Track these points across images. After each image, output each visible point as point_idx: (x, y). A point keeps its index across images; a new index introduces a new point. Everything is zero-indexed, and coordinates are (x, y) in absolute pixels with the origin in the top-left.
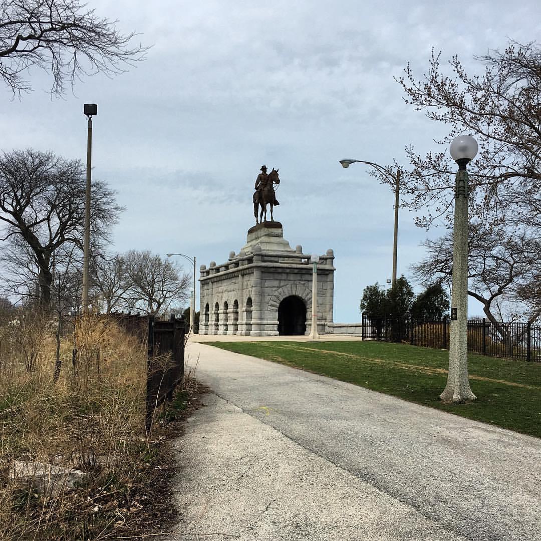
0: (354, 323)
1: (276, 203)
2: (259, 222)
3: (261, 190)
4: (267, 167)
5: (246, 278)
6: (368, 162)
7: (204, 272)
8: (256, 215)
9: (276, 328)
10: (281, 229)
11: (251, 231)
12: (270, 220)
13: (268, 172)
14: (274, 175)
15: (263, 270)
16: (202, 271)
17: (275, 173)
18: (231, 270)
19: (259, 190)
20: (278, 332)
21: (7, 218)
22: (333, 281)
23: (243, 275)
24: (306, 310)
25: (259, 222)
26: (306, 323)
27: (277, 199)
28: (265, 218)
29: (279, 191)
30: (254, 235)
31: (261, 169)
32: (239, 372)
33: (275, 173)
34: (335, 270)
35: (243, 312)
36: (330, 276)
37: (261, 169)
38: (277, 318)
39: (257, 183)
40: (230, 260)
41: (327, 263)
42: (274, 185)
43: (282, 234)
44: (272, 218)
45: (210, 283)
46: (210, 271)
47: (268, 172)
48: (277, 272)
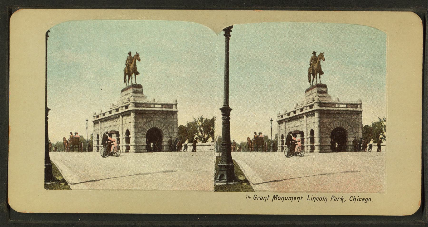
1: (137, 73)
3: (129, 65)
4: (131, 52)
10: (142, 89)
14: (322, 55)
16: (94, 115)
17: (322, 55)
18: (297, 114)
19: (127, 65)
20: (331, 150)
21: (125, 95)
23: (123, 117)
25: (312, 85)
26: (162, 144)
27: (138, 71)
29: (324, 66)
31: (312, 54)
33: (322, 55)
34: (178, 111)
37: (312, 54)
39: (311, 61)
44: (320, 82)
46: (284, 115)
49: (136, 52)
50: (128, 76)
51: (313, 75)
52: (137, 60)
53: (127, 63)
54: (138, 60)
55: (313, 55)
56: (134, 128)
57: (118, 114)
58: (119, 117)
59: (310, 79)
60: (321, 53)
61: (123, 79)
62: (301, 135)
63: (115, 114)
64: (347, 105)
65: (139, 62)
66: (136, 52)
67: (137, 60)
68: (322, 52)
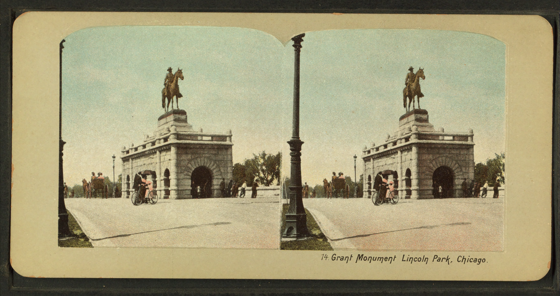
0: (500, 191)
1: (179, 96)
2: (408, 111)
3: (168, 85)
4: (172, 68)
5: (164, 153)
8: (405, 106)
13: (174, 72)
14: (421, 72)
16: (123, 150)
18: (389, 148)
19: (408, 85)
20: (433, 196)
23: (160, 152)
25: (408, 111)
26: (212, 188)
27: (180, 92)
28: (414, 106)
29: (424, 85)
32: (80, 223)
33: (421, 71)
35: (161, 180)
41: (214, 139)
42: (179, 81)
44: (419, 107)
47: (174, 72)
49: (179, 68)
52: (180, 78)
57: (154, 149)
58: (156, 152)
61: (161, 103)
63: (150, 149)
66: (179, 68)
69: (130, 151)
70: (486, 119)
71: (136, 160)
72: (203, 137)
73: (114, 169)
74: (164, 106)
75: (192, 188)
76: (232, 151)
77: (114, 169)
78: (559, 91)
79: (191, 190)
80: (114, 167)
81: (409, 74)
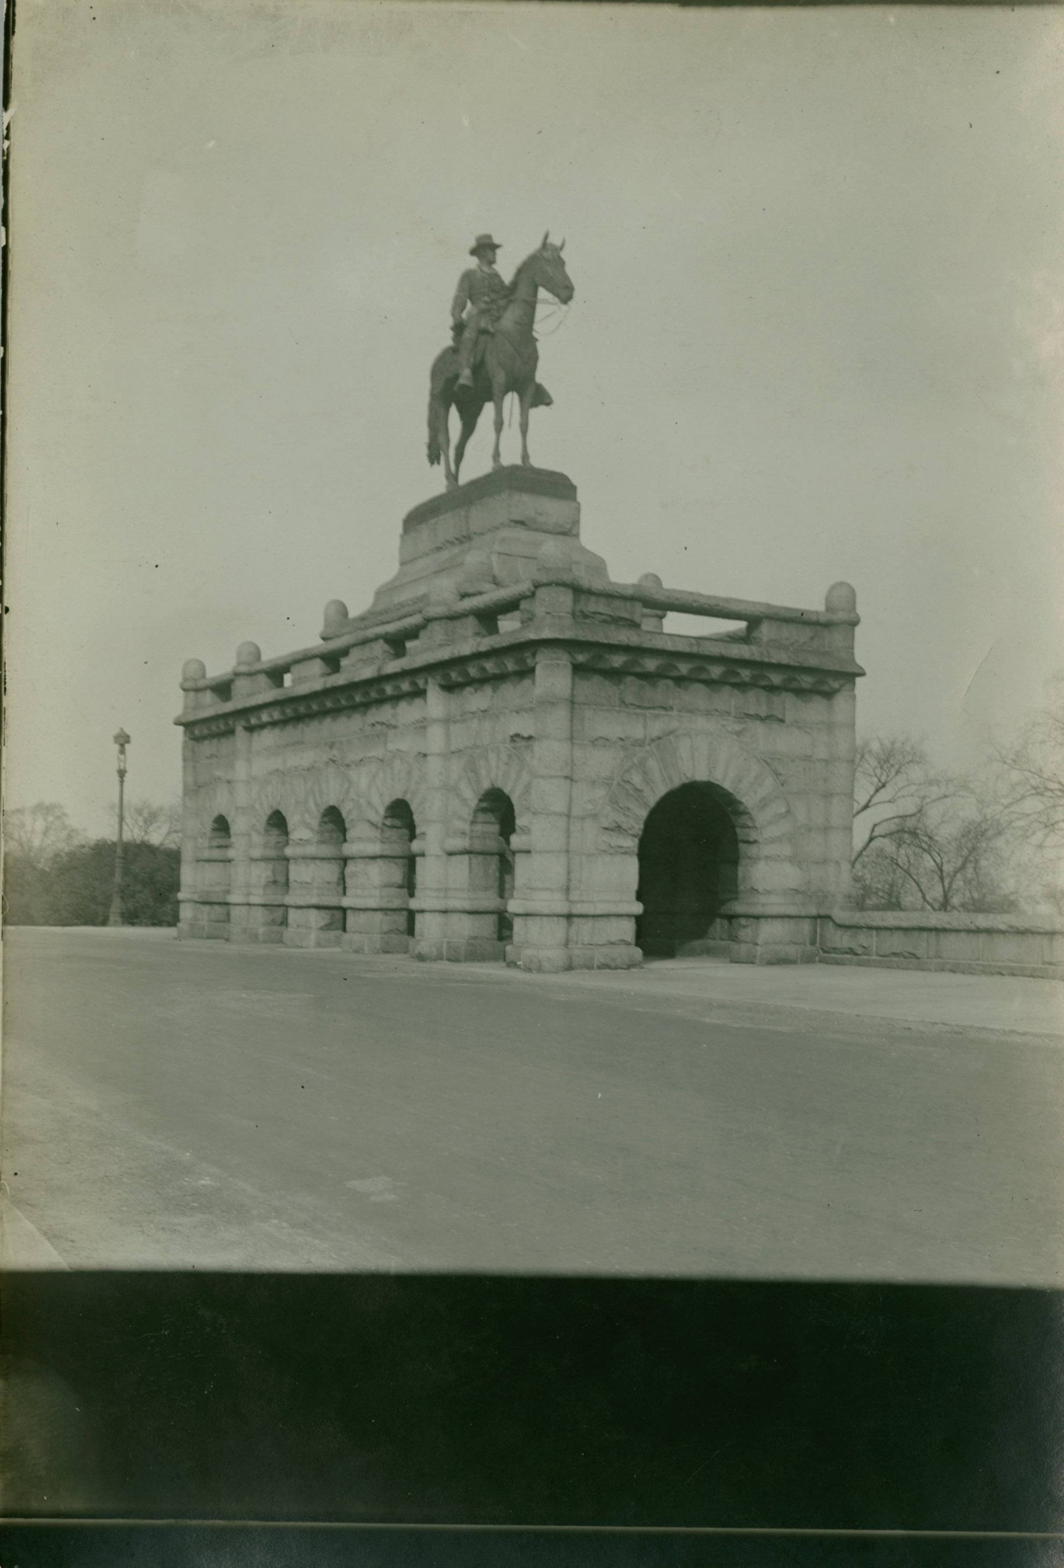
0: (237, 907)
1: (540, 397)
4: (496, 240)
6: (501, 449)
7: (197, 690)
9: (627, 930)
11: (416, 519)
12: (518, 461)
15: (581, 658)
20: (638, 952)
22: (853, 725)
24: (736, 850)
30: (425, 535)
34: (862, 674)
36: (840, 701)
38: (635, 886)
39: (458, 306)
40: (324, 639)
42: (541, 311)
43: (576, 522)
45: (239, 729)
47: (506, 268)
48: (601, 665)
49: (546, 237)
50: (462, 417)
51: (460, 411)
52: (551, 290)
53: (464, 315)
54: (557, 295)
55: (473, 262)
56: (753, 835)
57: (225, 716)
58: (232, 732)
59: (441, 438)
60: (544, 245)
61: (423, 434)
62: (508, 874)
63: (220, 712)
64: (754, 621)
65: (564, 307)
66: (546, 237)
67: (543, 293)
68: (550, 240)
69: (241, 686)
70: (876, 767)
71: (365, 714)
72: (671, 615)
73: (122, 782)
74: (434, 457)
75: (645, 911)
76: (854, 706)
77: (122, 782)
78: (2, 835)
79: (639, 919)
80: (122, 773)
81: (443, 683)
